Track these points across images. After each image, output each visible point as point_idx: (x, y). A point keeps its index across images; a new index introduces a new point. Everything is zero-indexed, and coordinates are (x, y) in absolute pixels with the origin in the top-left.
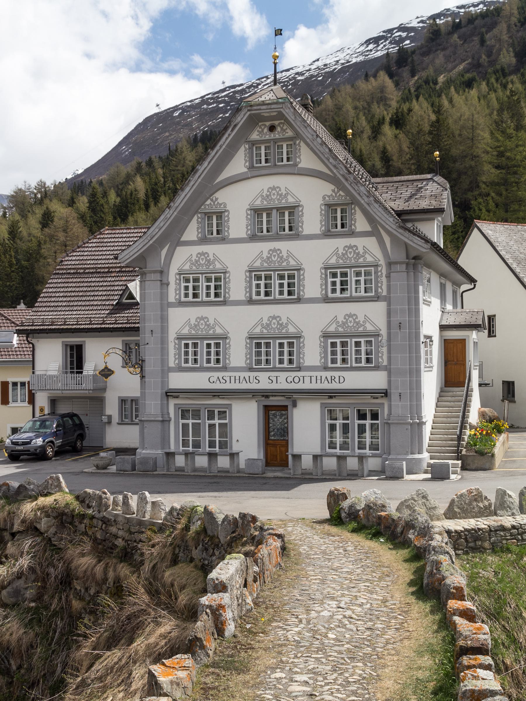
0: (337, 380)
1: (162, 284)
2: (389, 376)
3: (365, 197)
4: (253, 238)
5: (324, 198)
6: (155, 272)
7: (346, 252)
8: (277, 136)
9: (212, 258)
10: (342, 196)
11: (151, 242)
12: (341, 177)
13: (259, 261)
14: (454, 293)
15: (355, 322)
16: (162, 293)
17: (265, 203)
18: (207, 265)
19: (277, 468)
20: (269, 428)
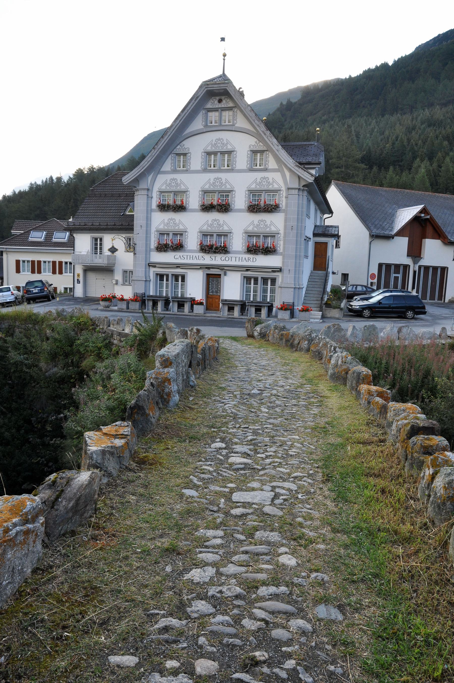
0: (251, 260)
1: (148, 197)
2: (283, 259)
3: (276, 146)
4: (205, 170)
5: (250, 147)
6: (144, 189)
7: (262, 181)
8: (223, 106)
9: (179, 182)
10: (261, 146)
11: (142, 170)
12: (261, 133)
13: (208, 185)
14: (321, 218)
15: (264, 225)
16: (147, 203)
17: (213, 148)
18: (176, 186)
19: (212, 312)
20: (209, 287)
